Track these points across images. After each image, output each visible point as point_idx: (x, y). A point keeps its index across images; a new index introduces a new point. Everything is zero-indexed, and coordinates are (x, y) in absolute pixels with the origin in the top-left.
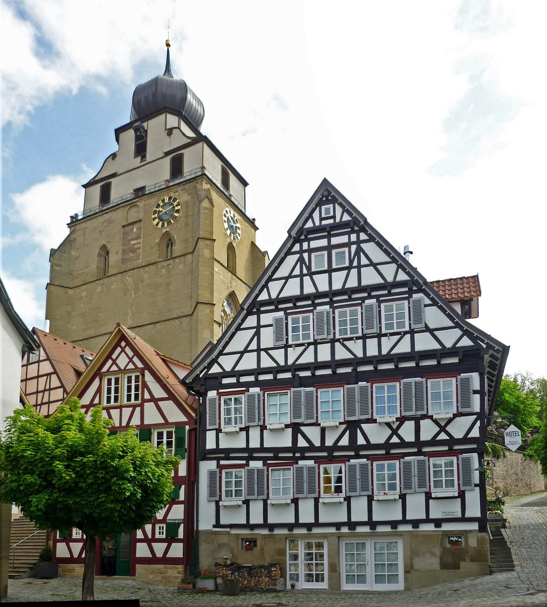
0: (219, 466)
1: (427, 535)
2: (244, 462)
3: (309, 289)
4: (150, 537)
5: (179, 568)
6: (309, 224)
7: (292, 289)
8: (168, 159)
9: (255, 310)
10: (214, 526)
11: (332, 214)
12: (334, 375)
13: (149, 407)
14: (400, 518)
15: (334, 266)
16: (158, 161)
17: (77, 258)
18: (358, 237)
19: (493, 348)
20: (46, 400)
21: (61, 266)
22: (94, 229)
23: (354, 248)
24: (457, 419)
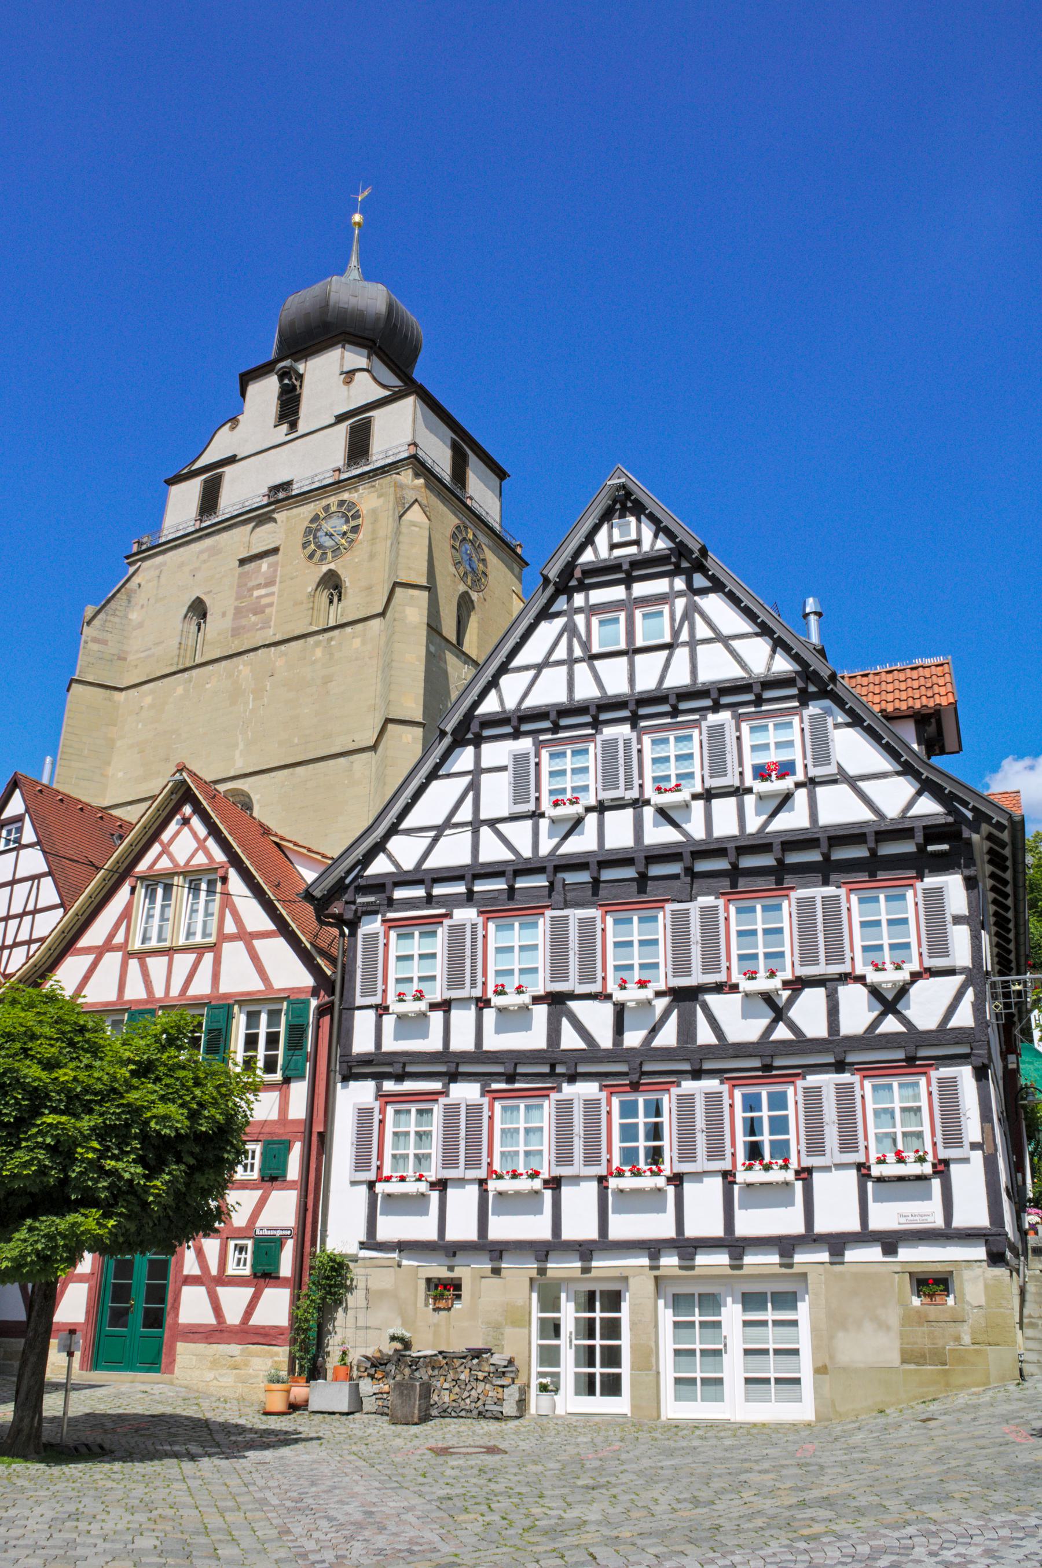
0: (380, 1095)
1: (865, 1274)
2: (437, 1086)
3: (586, 690)
4: (214, 1271)
5: (277, 1354)
6: (588, 556)
7: (550, 691)
8: (344, 427)
9: (470, 736)
10: (363, 1245)
11: (633, 536)
12: (638, 879)
13: (234, 953)
14: (800, 1229)
15: (640, 643)
16: (321, 432)
17: (140, 625)
18: (689, 583)
19: (988, 819)
20: (23, 936)
21: (104, 642)
22: (182, 565)
23: (680, 603)
24: (921, 984)
